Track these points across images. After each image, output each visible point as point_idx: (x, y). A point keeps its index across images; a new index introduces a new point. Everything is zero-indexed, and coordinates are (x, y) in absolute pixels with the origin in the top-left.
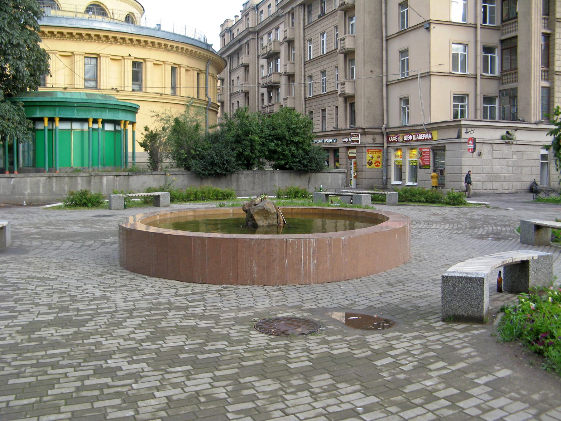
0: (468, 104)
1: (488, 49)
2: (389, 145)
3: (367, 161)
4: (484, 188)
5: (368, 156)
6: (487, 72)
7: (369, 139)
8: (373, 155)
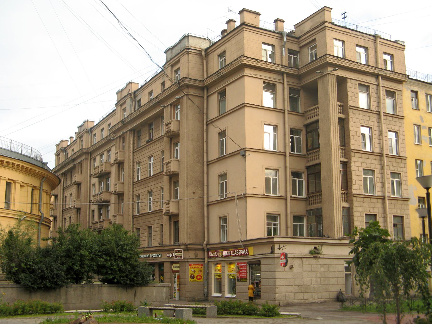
1: (296, 174)
3: (190, 275)
6: (296, 195)
7: (191, 255)
8: (195, 269)
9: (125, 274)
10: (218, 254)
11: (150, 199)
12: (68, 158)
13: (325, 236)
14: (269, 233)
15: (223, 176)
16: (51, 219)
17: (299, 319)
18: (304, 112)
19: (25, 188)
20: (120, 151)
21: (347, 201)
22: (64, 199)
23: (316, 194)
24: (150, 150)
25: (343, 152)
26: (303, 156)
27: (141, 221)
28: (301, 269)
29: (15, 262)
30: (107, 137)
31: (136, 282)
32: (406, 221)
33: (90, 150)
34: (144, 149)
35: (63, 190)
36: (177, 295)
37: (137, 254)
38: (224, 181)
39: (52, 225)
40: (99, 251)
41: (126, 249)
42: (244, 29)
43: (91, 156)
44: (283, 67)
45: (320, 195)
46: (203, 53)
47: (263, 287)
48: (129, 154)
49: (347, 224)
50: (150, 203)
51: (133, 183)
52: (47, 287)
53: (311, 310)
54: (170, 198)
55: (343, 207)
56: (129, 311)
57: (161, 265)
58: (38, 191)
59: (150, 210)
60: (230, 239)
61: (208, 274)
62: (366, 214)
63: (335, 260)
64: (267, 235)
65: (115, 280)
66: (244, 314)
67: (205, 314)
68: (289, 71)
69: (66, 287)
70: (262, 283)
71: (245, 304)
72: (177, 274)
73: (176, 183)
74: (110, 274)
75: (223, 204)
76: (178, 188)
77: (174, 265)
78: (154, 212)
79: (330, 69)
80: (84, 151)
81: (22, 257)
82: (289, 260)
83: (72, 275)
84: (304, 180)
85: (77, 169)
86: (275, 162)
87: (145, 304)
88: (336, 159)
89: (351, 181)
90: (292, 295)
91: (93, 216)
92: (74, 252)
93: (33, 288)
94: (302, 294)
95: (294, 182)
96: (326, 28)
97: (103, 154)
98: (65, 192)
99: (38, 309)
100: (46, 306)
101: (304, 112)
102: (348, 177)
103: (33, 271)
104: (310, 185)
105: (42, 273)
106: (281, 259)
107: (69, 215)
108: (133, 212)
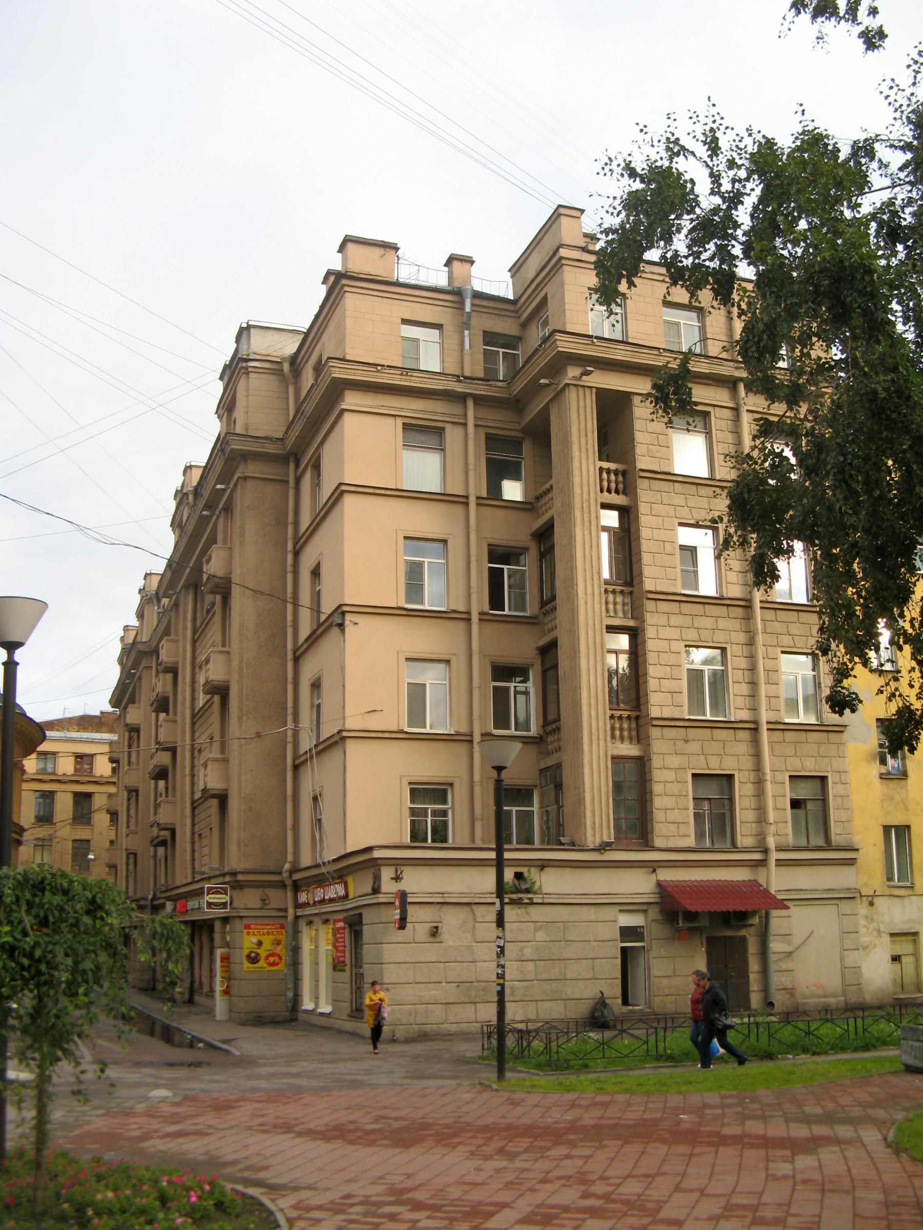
0: (453, 808)
1: (504, 672)
2: (300, 912)
3: (246, 952)
4: (452, 1018)
5: (249, 941)
6: (508, 728)
7: (249, 899)
8: (262, 938)
18: (533, 500)
26: (532, 621)
28: (469, 936)
32: (833, 790)
42: (346, 289)
44: (460, 381)
46: (286, 367)
62: (694, 775)
63: (584, 908)
68: (481, 390)
79: (573, 372)
88: (590, 621)
90: (438, 1011)
94: (473, 1006)
96: (564, 262)
101: (533, 500)
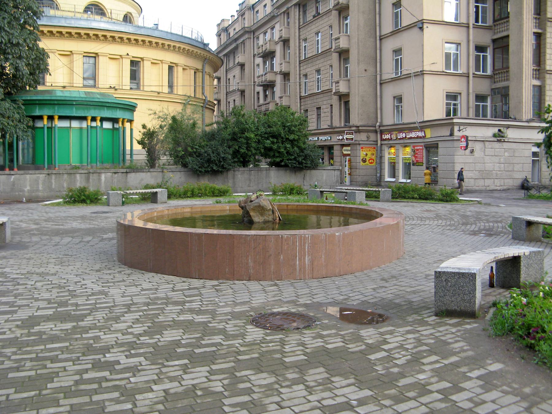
0: (460, 103)
1: (480, 49)
2: (383, 143)
3: (361, 158)
4: (477, 184)
5: (362, 154)
6: (479, 71)
7: (363, 137)
8: (367, 153)
9: (293, 157)
10: (392, 136)
11: (318, 78)
12: (230, 38)
13: (511, 118)
14: (448, 114)
15: (398, 52)
16: (216, 102)
17: (479, 205)
19: (188, 71)
20: (285, 28)
21: (538, 79)
22: (228, 82)
23: (502, 71)
24: (317, 25)
25: (537, 21)
26: (489, 28)
27: (309, 102)
29: (181, 146)
30: (270, 13)
31: (304, 165)
33: (253, 28)
34: (310, 25)
35: (226, 72)
36: (347, 179)
37: (306, 136)
38: (399, 57)
39: (216, 109)
40: (266, 133)
41: (294, 131)
43: (254, 34)
45: (507, 72)
47: (440, 172)
48: (295, 31)
49: (537, 104)
50: (318, 83)
51: (300, 61)
52: (214, 170)
53: (492, 197)
54: (340, 77)
55: (534, 86)
56: (298, 194)
57: (330, 148)
58: (201, 74)
59: (318, 90)
60: (405, 121)
61: (381, 157)
64: (446, 116)
65: (283, 164)
66: (420, 198)
67: (378, 198)
69: (234, 171)
70: (439, 168)
71: (421, 188)
72: (348, 158)
73: (346, 60)
74: (278, 157)
75: (397, 82)
76: (348, 65)
77: (345, 148)
78: (323, 92)
80: (247, 29)
81: (188, 141)
82: (470, 143)
83: (239, 159)
84: (489, 55)
85: (239, 49)
86: (457, 35)
87: (316, 186)
89: (545, 55)
91: (259, 98)
92: (239, 135)
93: (200, 172)
95: (477, 58)
97: (267, 32)
98: (228, 74)
99: (207, 192)
100: (214, 189)
102: (542, 51)
103: (200, 155)
104: (496, 60)
105: (208, 157)
106: (461, 142)
107: (233, 98)
108: (300, 92)
